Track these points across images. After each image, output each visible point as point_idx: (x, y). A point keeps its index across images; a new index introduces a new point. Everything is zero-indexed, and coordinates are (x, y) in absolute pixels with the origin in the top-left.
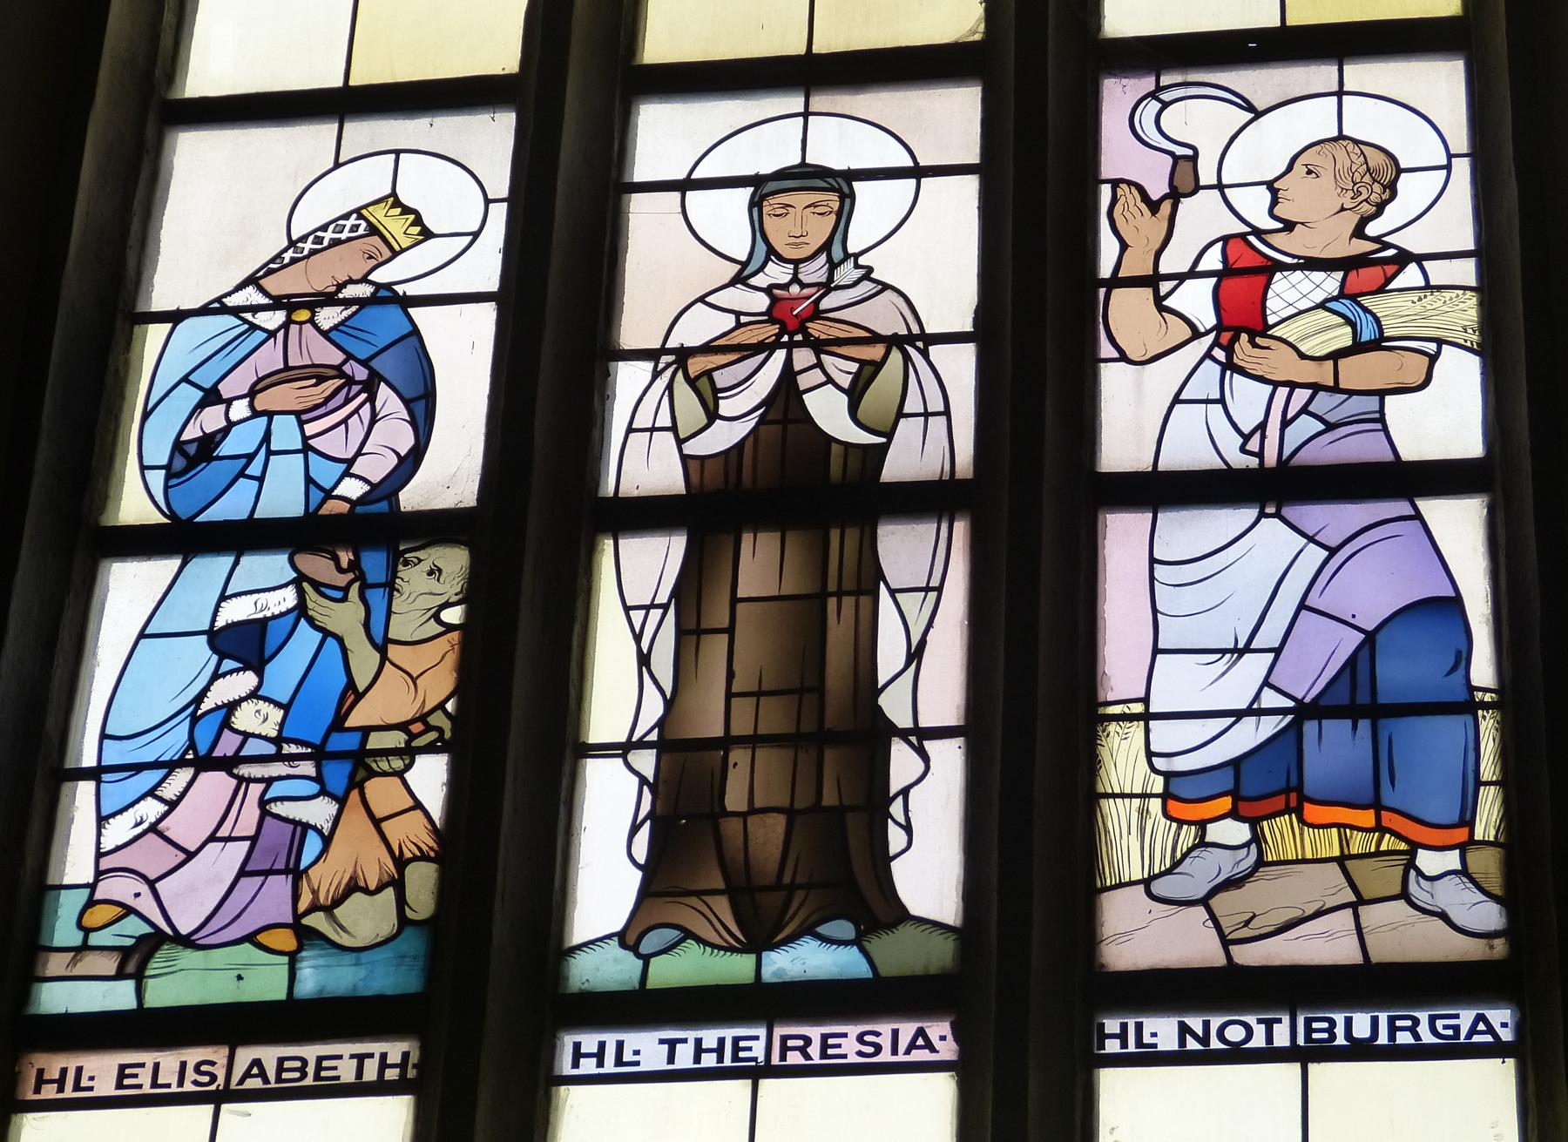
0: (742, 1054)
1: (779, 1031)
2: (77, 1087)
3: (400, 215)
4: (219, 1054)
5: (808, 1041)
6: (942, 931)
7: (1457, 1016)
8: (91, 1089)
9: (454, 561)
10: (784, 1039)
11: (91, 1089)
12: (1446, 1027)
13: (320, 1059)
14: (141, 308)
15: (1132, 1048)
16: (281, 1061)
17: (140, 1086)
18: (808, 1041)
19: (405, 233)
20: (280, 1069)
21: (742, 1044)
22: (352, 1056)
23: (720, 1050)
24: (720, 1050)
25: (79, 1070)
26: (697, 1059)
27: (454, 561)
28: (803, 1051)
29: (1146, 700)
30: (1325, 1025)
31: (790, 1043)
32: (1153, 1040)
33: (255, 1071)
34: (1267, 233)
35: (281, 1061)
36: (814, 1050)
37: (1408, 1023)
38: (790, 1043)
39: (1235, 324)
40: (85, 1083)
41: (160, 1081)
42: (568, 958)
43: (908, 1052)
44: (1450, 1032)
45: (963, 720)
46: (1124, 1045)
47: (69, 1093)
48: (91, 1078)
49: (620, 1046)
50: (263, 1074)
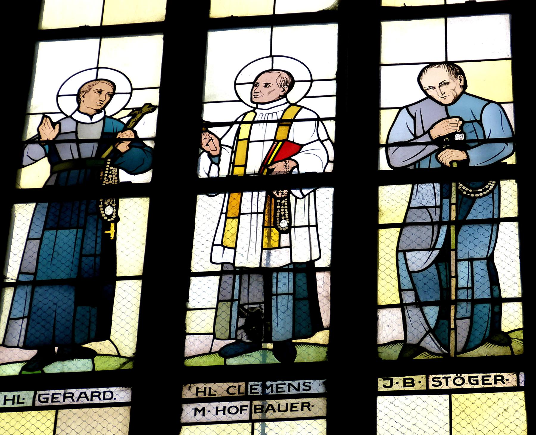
0: (253, 391)
3: (209, 146)
4: (243, 384)
6: (386, 346)
7: (477, 377)
8: (23, 403)
10: (251, 386)
11: (23, 403)
12: (44, 398)
15: (207, 396)
16: (92, 393)
18: (100, 393)
19: (217, 150)
20: (92, 396)
21: (485, 378)
22: (443, 378)
23: (13, 400)
24: (205, 392)
26: (197, 395)
28: (98, 396)
30: (410, 381)
32: (215, 393)
34: (332, 142)
35: (92, 393)
36: (101, 396)
37: (500, 378)
39: (237, 152)
40: (21, 401)
42: (74, 359)
43: (78, 401)
44: (475, 382)
45: (142, 274)
46: (205, 395)
48: (24, 399)
49: (210, 388)
50: (86, 397)
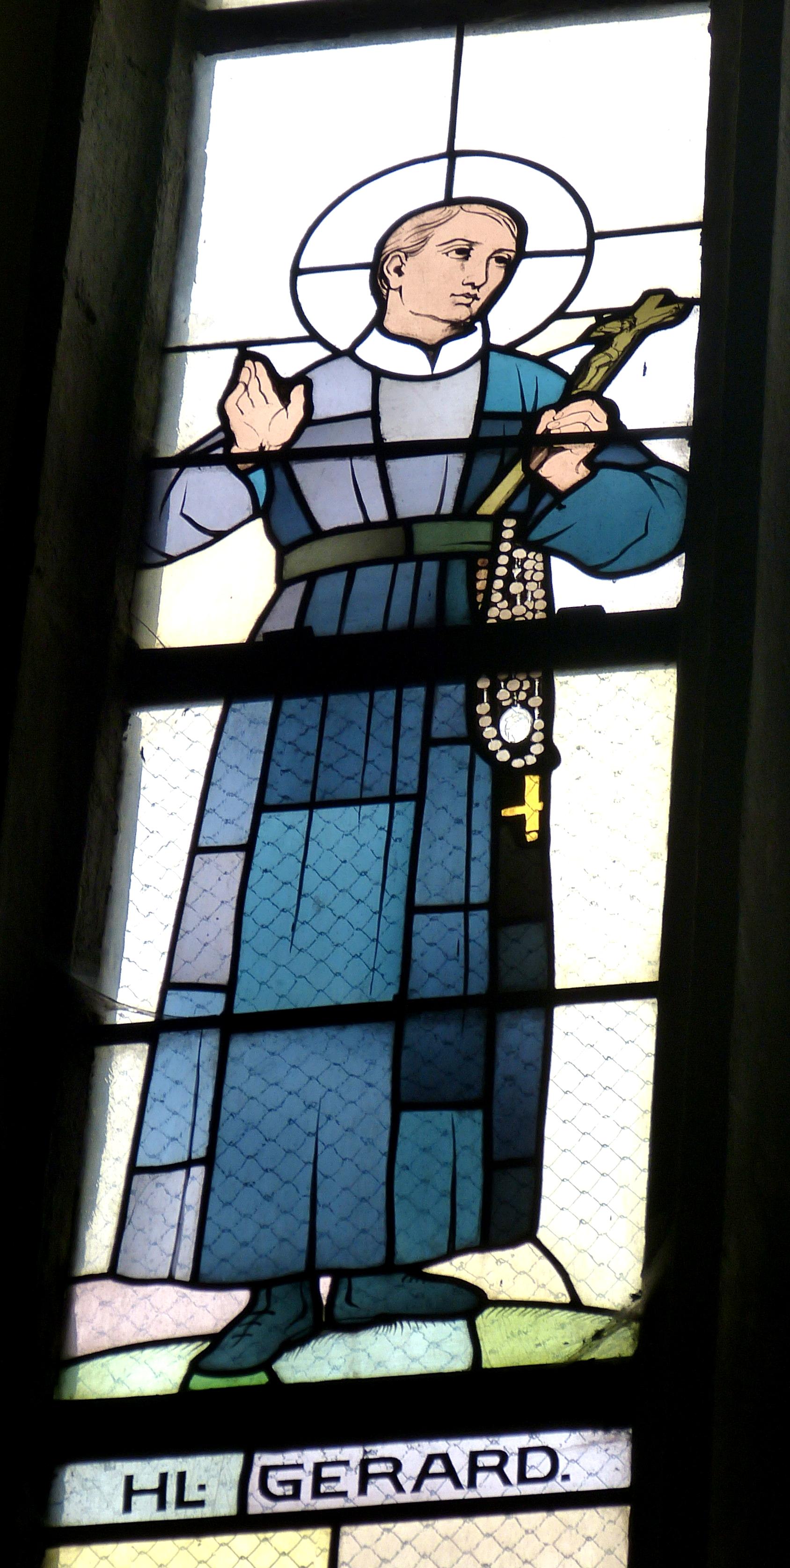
1: (262, 1459)
2: (181, 1503)
5: (504, 1457)
8: (200, 1503)
9: (484, 914)
10: (265, 1470)
11: (200, 1503)
13: (318, 1467)
14: (173, 344)
17: (344, 1494)
25: (182, 1476)
27: (484, 914)
28: (499, 1469)
29: (229, 989)
31: (482, 1461)
33: (438, 1467)
35: (474, 1456)
38: (482, 1461)
40: (191, 1495)
41: (529, 1475)
43: (417, 1488)
47: (172, 1513)
50: (450, 1472)
